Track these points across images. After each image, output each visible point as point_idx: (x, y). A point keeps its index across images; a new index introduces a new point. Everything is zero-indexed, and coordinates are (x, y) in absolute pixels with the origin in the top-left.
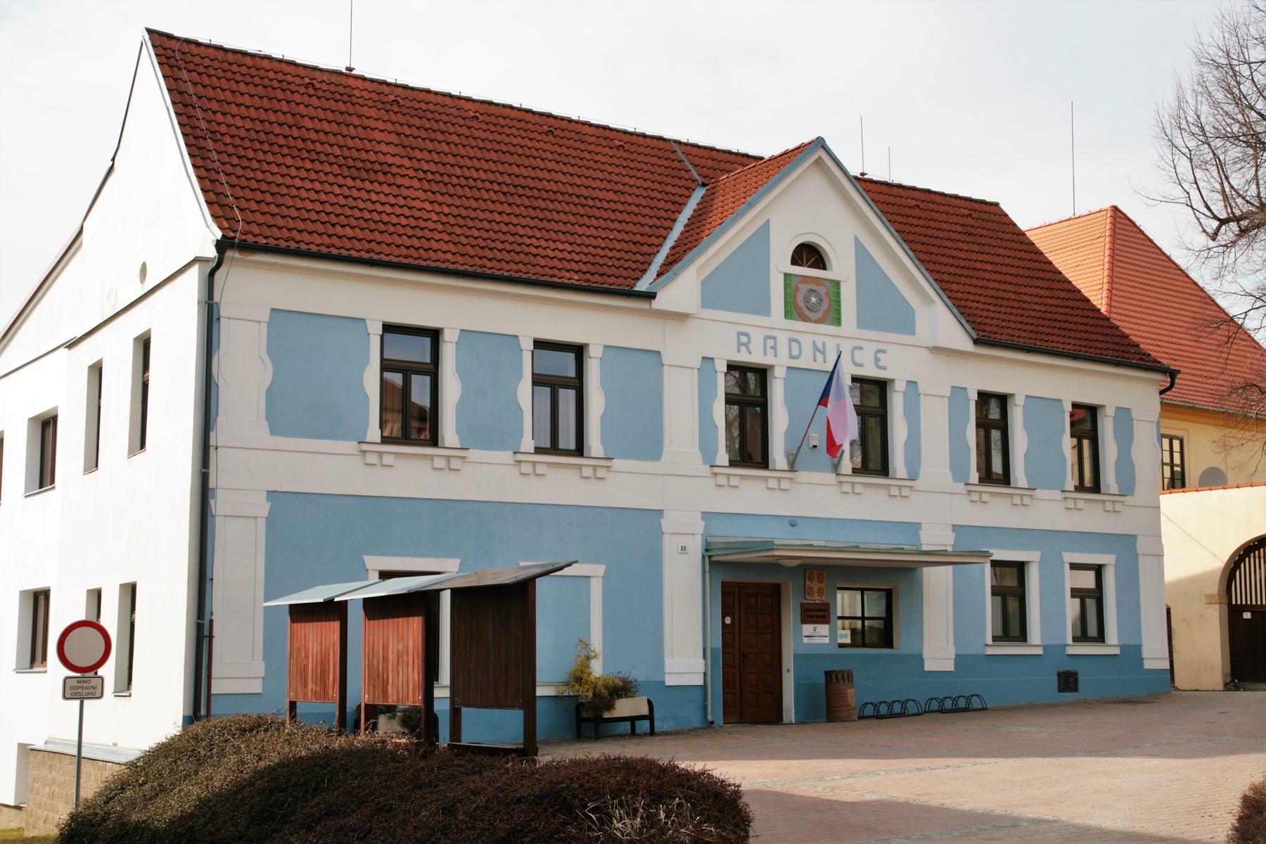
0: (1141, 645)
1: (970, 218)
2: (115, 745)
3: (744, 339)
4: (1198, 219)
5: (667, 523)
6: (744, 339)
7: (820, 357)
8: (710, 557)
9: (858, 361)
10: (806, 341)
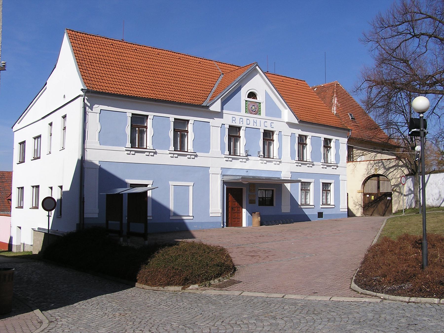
0: (12, 172)
1: (283, 82)
2: (57, 230)
3: (234, 119)
4: (239, 67)
5: (210, 171)
6: (234, 119)
7: (255, 124)
8: (223, 180)
9: (265, 125)
10: (252, 120)
